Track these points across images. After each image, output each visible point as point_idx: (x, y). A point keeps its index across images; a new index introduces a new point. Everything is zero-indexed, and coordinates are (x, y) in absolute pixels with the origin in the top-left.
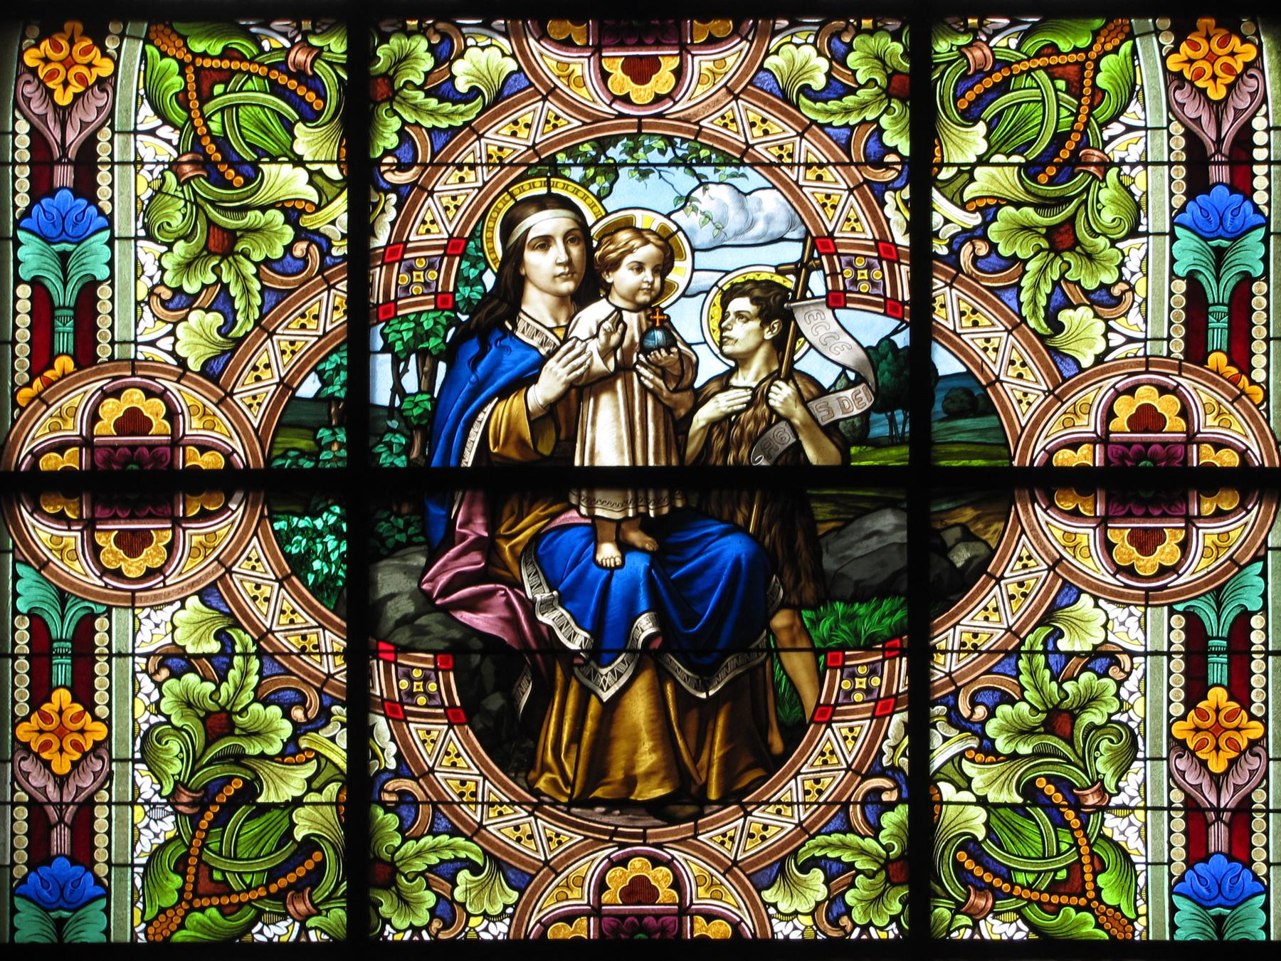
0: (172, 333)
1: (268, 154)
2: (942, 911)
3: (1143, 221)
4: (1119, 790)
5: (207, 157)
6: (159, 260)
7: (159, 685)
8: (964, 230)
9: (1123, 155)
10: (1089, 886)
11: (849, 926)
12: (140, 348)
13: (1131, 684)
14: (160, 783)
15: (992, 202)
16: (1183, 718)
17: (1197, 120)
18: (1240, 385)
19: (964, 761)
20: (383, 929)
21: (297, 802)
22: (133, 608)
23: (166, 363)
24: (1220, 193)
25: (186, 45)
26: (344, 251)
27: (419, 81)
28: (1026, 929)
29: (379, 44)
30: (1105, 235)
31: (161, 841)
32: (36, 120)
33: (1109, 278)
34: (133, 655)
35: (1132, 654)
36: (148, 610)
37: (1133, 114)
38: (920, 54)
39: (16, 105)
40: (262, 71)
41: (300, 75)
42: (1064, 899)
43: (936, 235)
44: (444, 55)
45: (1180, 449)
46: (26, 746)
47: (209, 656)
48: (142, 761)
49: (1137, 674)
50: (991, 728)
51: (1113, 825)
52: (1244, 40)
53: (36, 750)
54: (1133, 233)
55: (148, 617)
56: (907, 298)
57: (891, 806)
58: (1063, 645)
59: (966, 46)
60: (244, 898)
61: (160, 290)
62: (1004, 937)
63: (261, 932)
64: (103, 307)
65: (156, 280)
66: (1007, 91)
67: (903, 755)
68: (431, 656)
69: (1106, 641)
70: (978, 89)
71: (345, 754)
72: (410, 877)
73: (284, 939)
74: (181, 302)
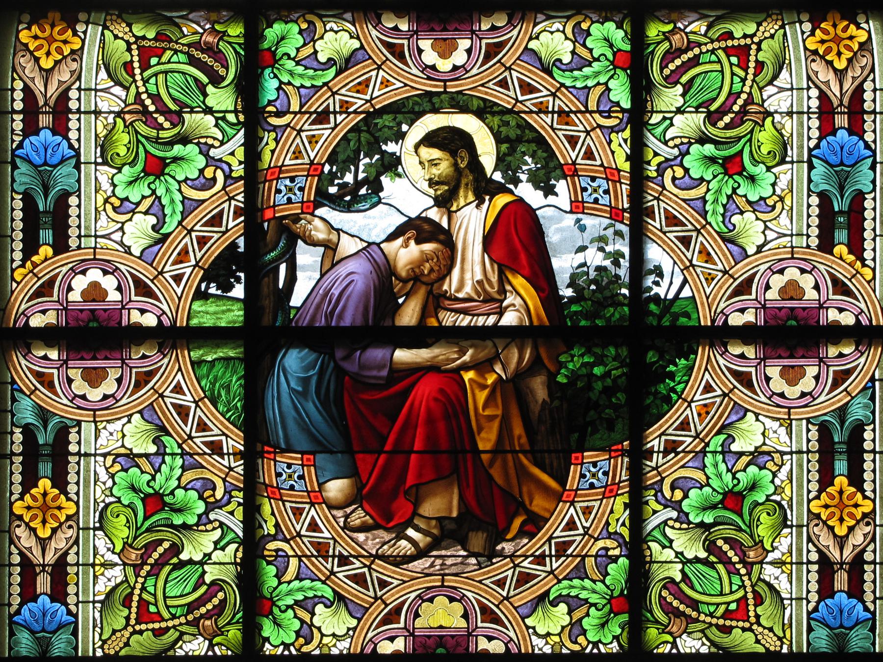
0: (121, 229)
1: (187, 106)
2: (652, 632)
3: (789, 153)
4: (774, 549)
5: (145, 107)
6: (112, 179)
7: (112, 476)
8: (220, 508)
9: (776, 108)
10: (752, 614)
11: (585, 643)
12: (99, 240)
13: (783, 474)
14: (113, 543)
15: (202, 528)
16: (818, 497)
17: (827, 83)
18: (856, 267)
19: (667, 528)
20: (263, 646)
21: (679, 111)
22: (792, 247)
23: (117, 250)
24: (842, 135)
25: (131, 31)
26: (241, 173)
27: (593, 609)
28: (708, 644)
29: (267, 28)
30: (763, 163)
31: (113, 584)
32: (27, 81)
33: (767, 192)
34: (95, 455)
35: (782, 454)
36: (105, 423)
37: (784, 78)
38: (638, 38)
39: (14, 70)
40: (702, 617)
41: (209, 49)
42: (734, 623)
43: (239, 504)
44: (310, 36)
45: (71, 356)
46: (20, 518)
47: (147, 456)
48: (101, 528)
49: (785, 469)
50: (201, 161)
51: (769, 572)
52: (858, 27)
53: (27, 520)
54: (783, 162)
55: (105, 428)
56: (626, 206)
57: (615, 559)
58: (734, 447)
59: (669, 32)
60: (716, 45)
61: (774, 469)
62: (694, 651)
63: (181, 648)
64: (73, 211)
65: (109, 193)
66: (698, 64)
67: (623, 524)
68: (300, 456)
69: (764, 444)
70: (678, 62)
71: (242, 525)
72: (283, 608)
73: (196, 653)
74: (758, 456)
